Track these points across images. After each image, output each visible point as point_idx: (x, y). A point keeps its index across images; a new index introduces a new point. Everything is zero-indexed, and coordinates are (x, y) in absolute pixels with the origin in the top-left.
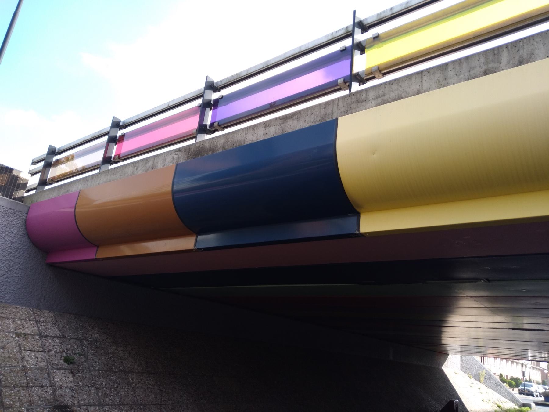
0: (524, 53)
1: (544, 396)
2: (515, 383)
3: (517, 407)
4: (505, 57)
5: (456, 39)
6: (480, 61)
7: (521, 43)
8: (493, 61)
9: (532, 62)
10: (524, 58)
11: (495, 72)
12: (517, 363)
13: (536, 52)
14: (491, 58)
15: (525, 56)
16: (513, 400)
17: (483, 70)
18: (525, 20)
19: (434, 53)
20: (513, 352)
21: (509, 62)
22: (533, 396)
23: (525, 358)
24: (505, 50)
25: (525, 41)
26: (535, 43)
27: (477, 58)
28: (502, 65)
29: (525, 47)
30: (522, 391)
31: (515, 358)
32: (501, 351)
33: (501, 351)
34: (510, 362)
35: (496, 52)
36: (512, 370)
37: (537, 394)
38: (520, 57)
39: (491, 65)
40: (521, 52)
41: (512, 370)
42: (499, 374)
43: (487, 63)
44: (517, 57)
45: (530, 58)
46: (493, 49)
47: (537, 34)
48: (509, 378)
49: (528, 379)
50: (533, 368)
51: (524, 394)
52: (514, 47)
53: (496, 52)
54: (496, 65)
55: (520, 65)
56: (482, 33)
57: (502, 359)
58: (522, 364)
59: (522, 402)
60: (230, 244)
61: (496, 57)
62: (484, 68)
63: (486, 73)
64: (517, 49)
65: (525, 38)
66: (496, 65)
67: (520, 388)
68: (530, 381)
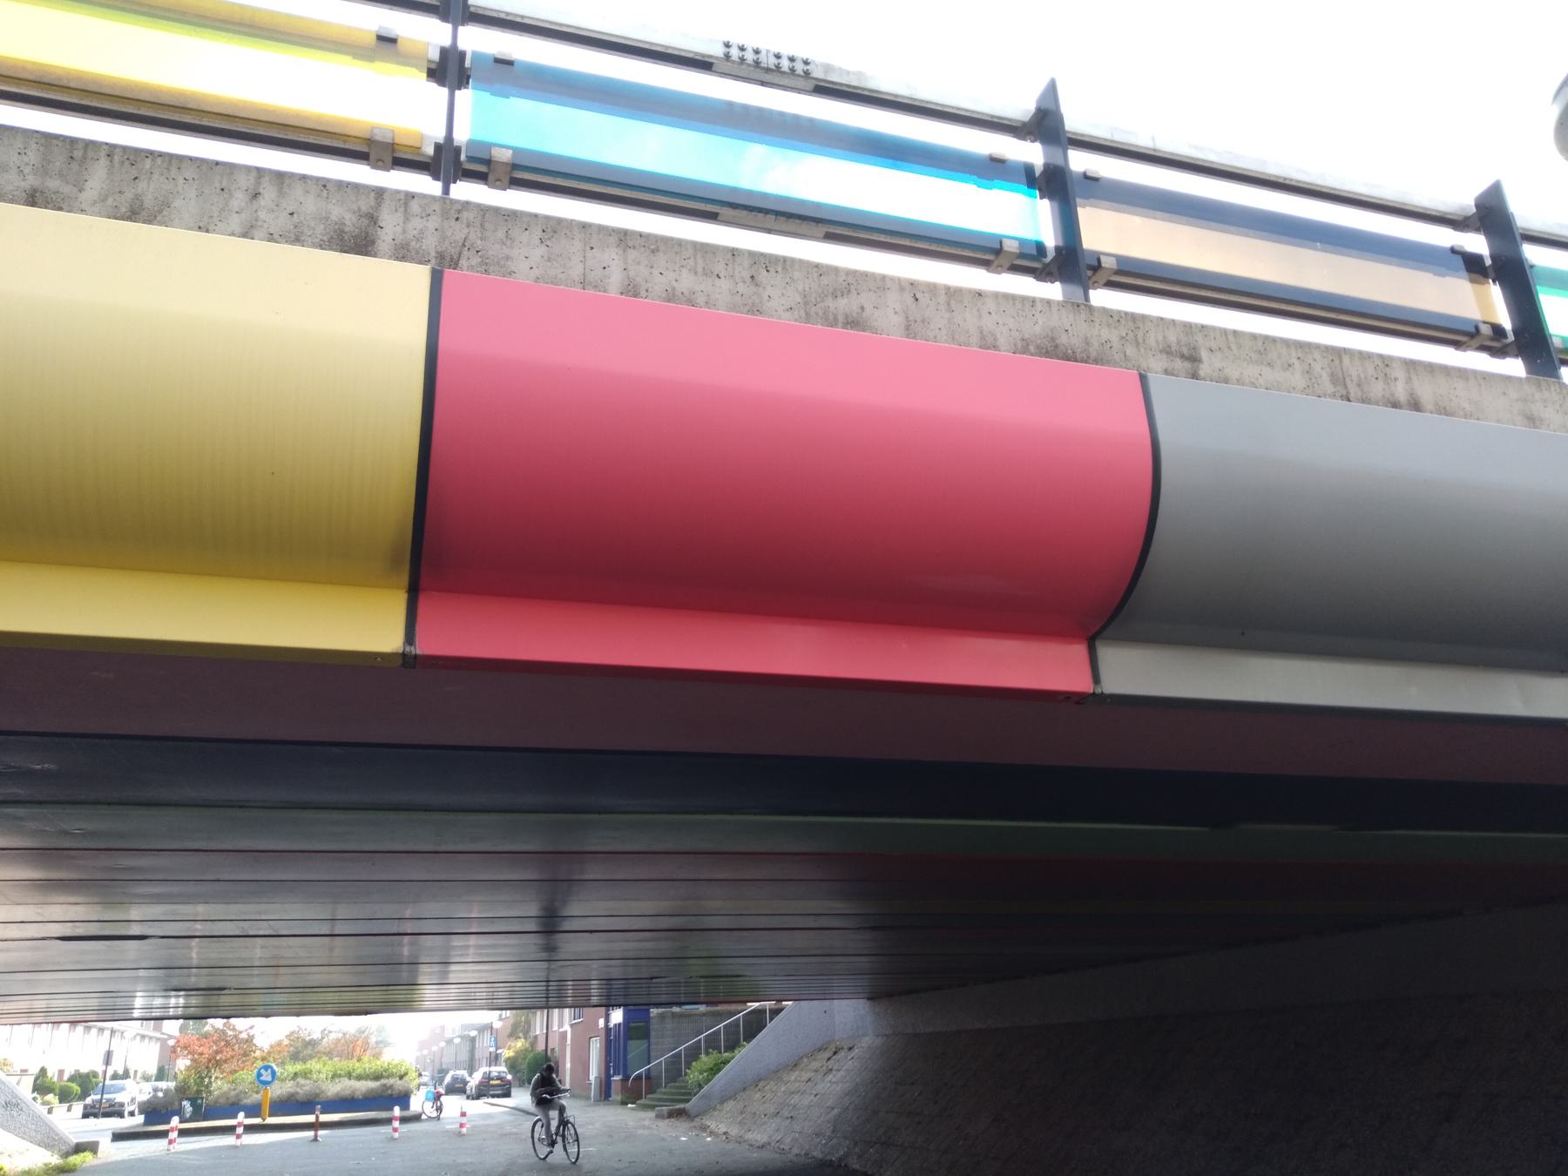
0: (149, 190)
1: (141, 1113)
2: (80, 1089)
3: (54, 1160)
4: (97, 178)
5: (80, 76)
6: (26, 159)
7: (148, 163)
8: (61, 175)
9: (161, 224)
10: (146, 205)
11: (60, 209)
12: (101, 1030)
13: (178, 203)
14: (59, 161)
15: (149, 201)
16: (49, 1140)
17: (26, 185)
18: (184, 109)
19: (18, 85)
20: (93, 1002)
21: (104, 200)
22: (121, 1115)
23: (124, 1014)
24: (103, 161)
25: (159, 160)
26: (181, 181)
27: (19, 143)
28: (84, 196)
29: (155, 177)
30: (93, 1107)
31: (94, 1017)
32: (58, 1003)
33: (58, 1003)
34: (94, 1031)
35: (78, 154)
36: (72, 1050)
37: (131, 1108)
38: (137, 197)
39: (53, 184)
40: (142, 185)
41: (72, 1050)
42: (35, 1070)
43: (43, 170)
44: (129, 195)
45: (160, 211)
46: (72, 142)
47: (191, 159)
48: (66, 1077)
49: (121, 1072)
50: (143, 1037)
51: (96, 1116)
52: (127, 163)
53: (78, 154)
54: (67, 189)
55: (129, 219)
56: (64, 83)
57: (74, 1023)
58: (113, 1032)
59: (75, 1140)
60: (407, 567)
61: (75, 166)
62: (32, 181)
63: (33, 199)
64: (134, 173)
65: (161, 155)
66: (67, 189)
67: (89, 1100)
68: (126, 1075)
